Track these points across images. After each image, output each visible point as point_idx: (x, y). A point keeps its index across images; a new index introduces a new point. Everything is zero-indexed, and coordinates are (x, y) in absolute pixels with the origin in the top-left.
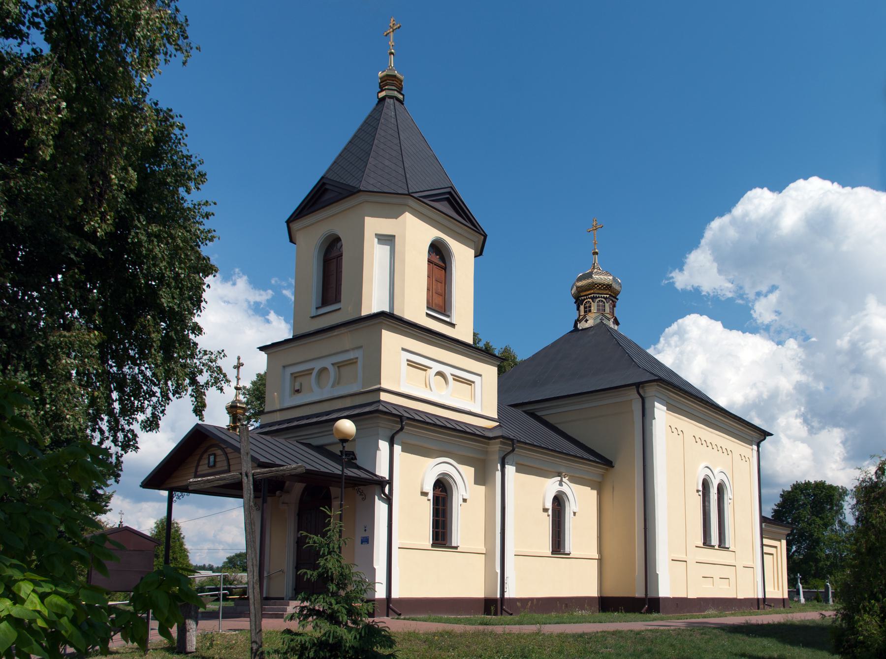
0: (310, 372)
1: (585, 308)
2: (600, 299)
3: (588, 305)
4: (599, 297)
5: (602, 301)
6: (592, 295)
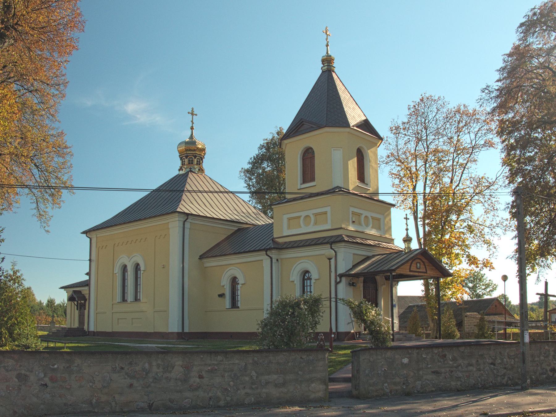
1: (189, 161)
4: (189, 156)
5: (192, 158)
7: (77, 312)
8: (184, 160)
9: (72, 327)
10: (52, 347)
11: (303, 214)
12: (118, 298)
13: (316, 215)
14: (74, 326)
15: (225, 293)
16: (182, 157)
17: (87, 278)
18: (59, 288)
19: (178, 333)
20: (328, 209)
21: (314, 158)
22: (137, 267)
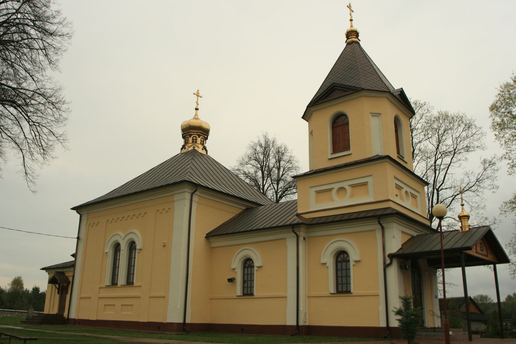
0: (331, 190)
1: (193, 139)
2: (195, 135)
3: (195, 138)
4: (193, 134)
5: (196, 136)
6: (199, 134)
7: (57, 297)
8: (187, 139)
9: (51, 313)
10: (240, 179)
11: (336, 186)
12: (108, 281)
13: (353, 186)
14: (52, 312)
15: (235, 278)
16: (186, 136)
17: (73, 259)
18: (41, 269)
19: (178, 324)
20: (369, 180)
21: (349, 125)
22: (132, 245)
